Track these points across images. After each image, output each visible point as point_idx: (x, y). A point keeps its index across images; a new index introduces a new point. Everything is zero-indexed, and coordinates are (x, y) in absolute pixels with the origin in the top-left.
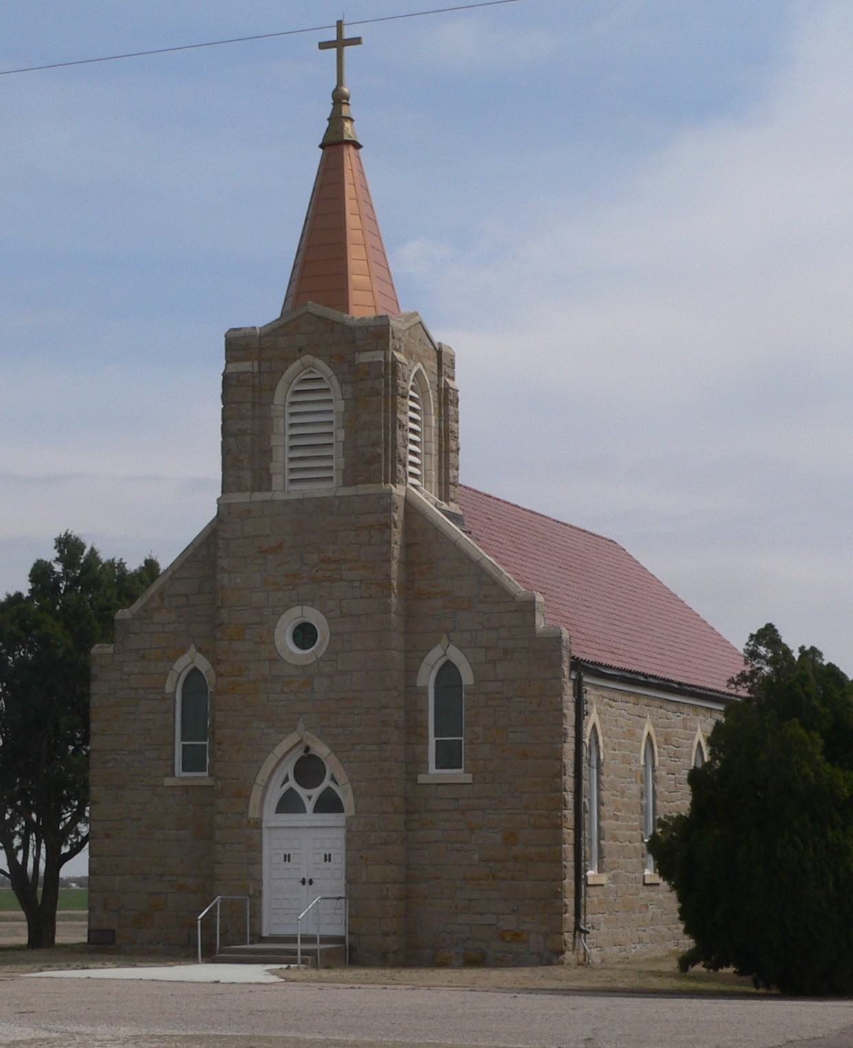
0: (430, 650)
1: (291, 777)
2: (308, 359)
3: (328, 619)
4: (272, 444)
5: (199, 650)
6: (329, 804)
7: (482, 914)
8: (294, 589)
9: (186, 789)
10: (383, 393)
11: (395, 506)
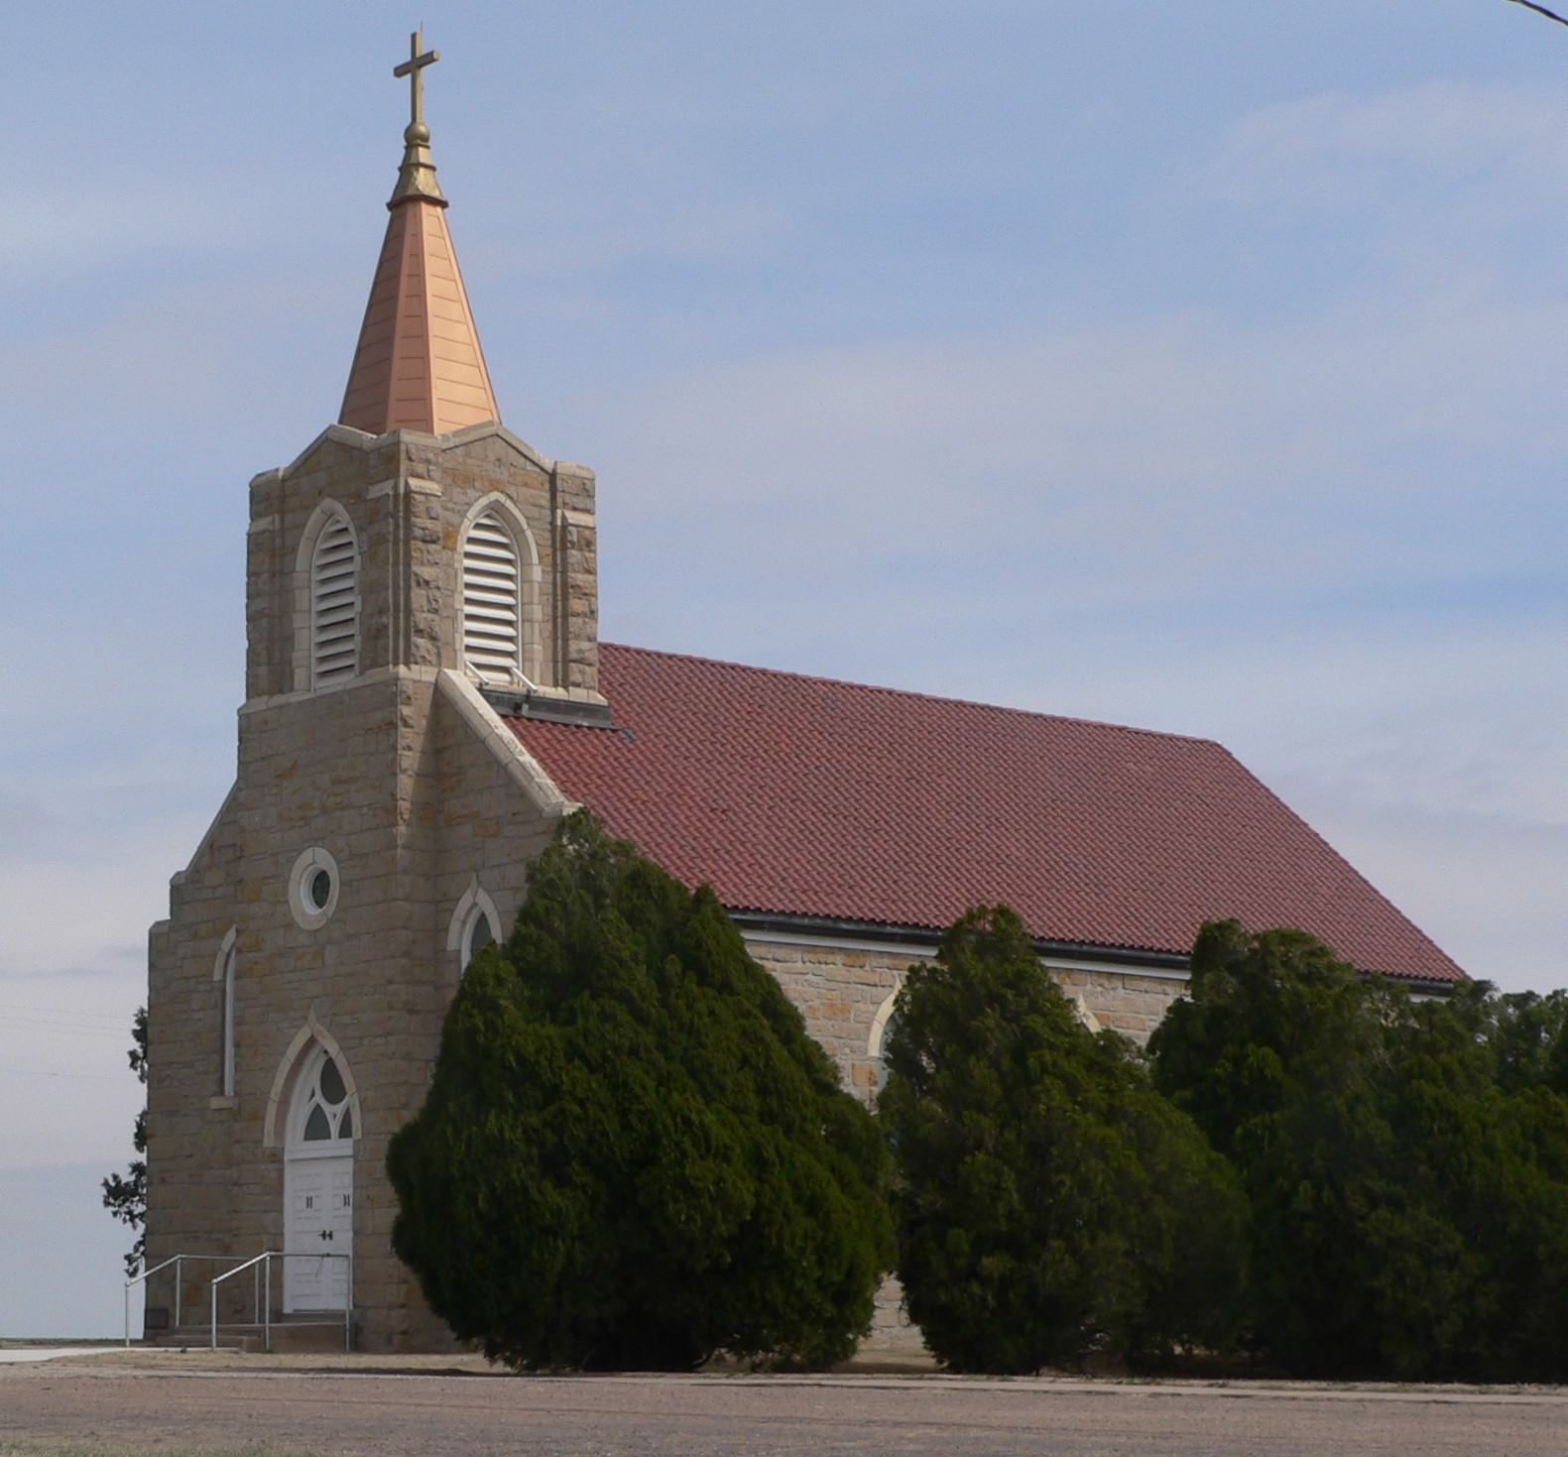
1: (318, 1092)
8: (306, 825)
10: (391, 538)
11: (404, 696)
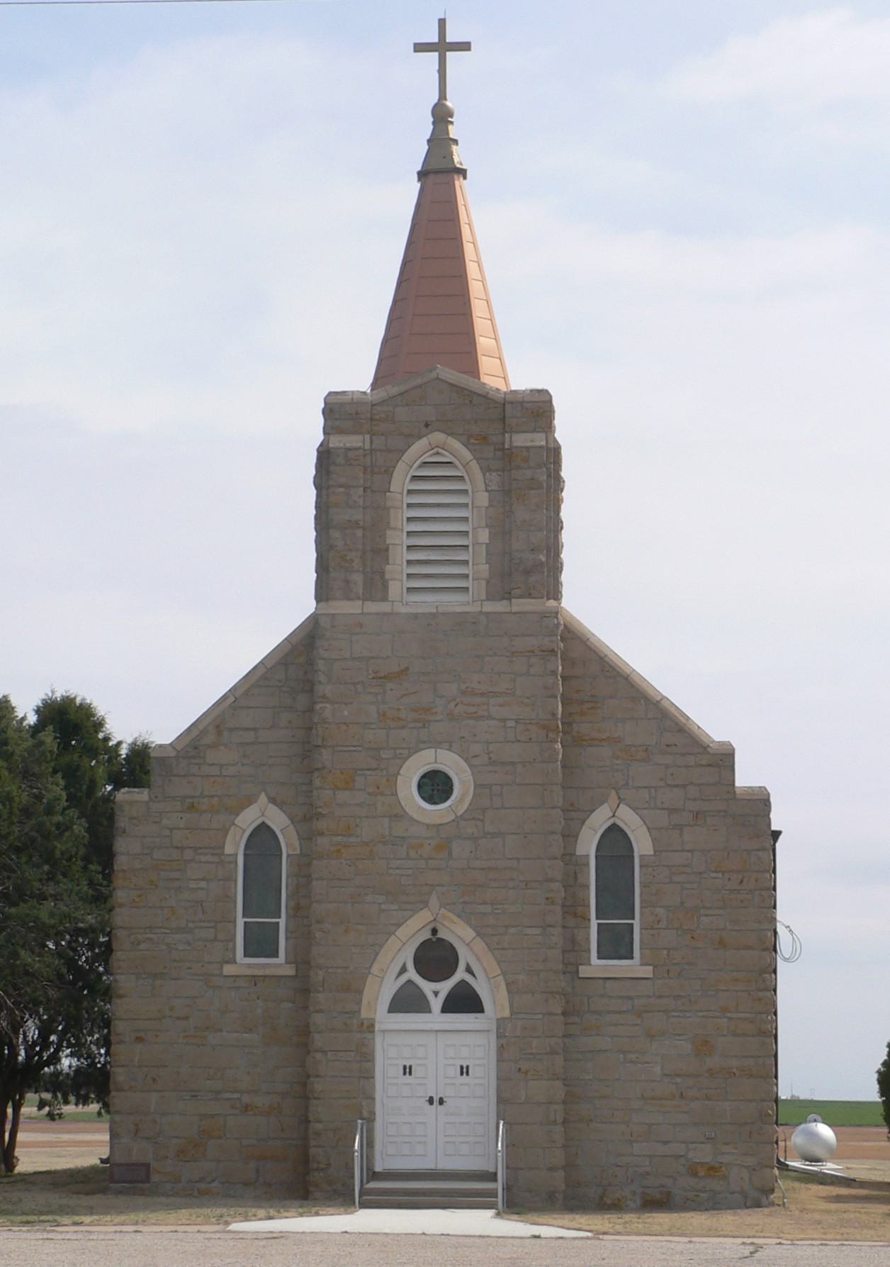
0: (592, 811)
2: (438, 437)
3: (471, 766)
4: (388, 542)
5: (273, 800)
6: (462, 1001)
7: (665, 1143)
8: (424, 727)
9: (254, 979)
